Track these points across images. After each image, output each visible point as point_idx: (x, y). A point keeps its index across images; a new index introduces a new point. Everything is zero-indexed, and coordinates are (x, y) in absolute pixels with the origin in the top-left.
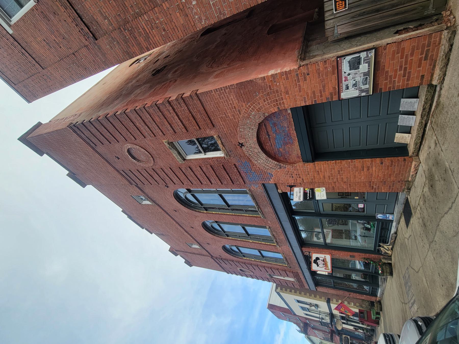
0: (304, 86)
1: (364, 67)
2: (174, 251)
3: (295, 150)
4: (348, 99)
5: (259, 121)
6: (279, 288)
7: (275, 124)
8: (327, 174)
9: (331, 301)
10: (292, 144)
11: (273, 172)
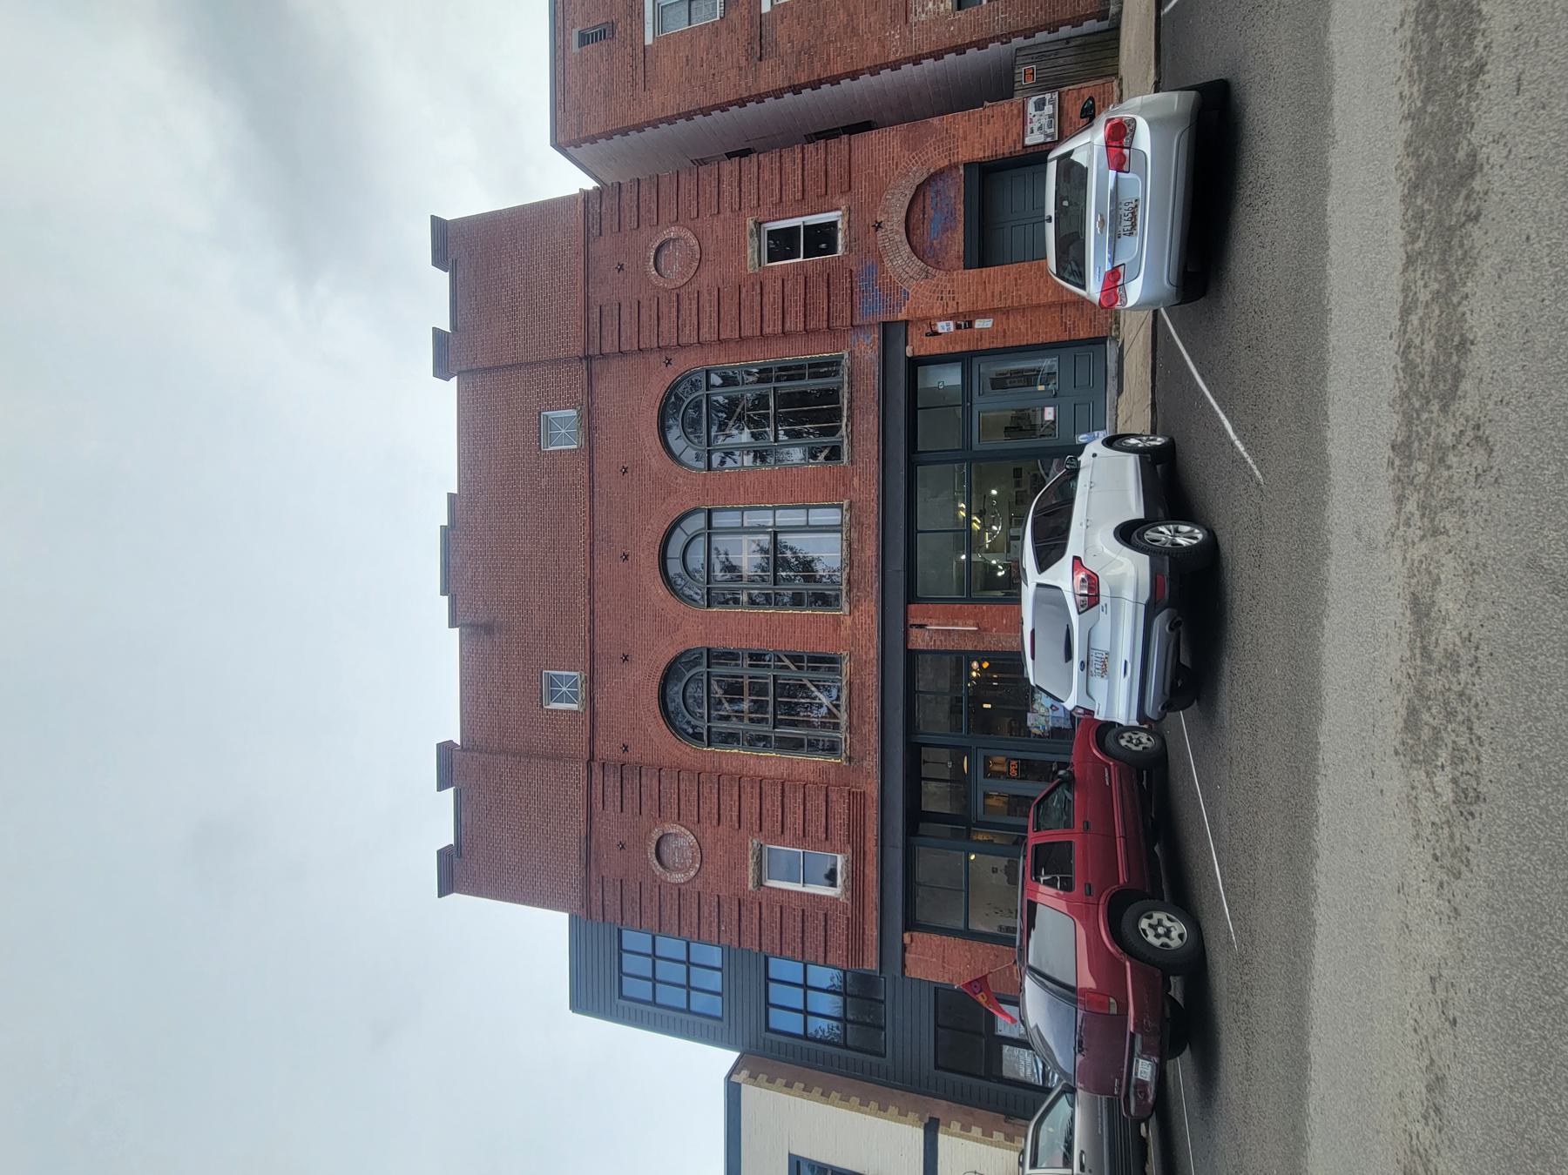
0: (987, 130)
1: (1048, 109)
2: (451, 766)
3: (956, 242)
4: (937, 1025)
5: (918, 182)
6: (745, 1073)
7: (938, 193)
8: (998, 288)
9: (941, 1128)
10: (954, 230)
11: (911, 287)
